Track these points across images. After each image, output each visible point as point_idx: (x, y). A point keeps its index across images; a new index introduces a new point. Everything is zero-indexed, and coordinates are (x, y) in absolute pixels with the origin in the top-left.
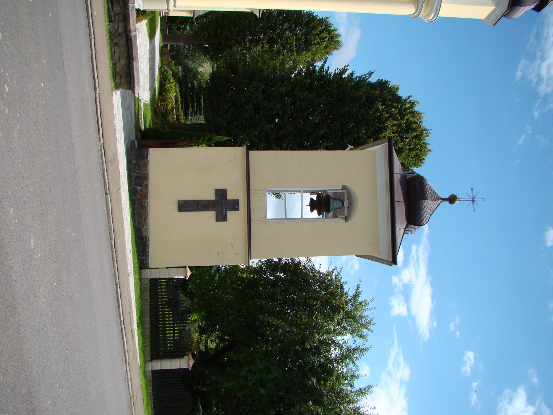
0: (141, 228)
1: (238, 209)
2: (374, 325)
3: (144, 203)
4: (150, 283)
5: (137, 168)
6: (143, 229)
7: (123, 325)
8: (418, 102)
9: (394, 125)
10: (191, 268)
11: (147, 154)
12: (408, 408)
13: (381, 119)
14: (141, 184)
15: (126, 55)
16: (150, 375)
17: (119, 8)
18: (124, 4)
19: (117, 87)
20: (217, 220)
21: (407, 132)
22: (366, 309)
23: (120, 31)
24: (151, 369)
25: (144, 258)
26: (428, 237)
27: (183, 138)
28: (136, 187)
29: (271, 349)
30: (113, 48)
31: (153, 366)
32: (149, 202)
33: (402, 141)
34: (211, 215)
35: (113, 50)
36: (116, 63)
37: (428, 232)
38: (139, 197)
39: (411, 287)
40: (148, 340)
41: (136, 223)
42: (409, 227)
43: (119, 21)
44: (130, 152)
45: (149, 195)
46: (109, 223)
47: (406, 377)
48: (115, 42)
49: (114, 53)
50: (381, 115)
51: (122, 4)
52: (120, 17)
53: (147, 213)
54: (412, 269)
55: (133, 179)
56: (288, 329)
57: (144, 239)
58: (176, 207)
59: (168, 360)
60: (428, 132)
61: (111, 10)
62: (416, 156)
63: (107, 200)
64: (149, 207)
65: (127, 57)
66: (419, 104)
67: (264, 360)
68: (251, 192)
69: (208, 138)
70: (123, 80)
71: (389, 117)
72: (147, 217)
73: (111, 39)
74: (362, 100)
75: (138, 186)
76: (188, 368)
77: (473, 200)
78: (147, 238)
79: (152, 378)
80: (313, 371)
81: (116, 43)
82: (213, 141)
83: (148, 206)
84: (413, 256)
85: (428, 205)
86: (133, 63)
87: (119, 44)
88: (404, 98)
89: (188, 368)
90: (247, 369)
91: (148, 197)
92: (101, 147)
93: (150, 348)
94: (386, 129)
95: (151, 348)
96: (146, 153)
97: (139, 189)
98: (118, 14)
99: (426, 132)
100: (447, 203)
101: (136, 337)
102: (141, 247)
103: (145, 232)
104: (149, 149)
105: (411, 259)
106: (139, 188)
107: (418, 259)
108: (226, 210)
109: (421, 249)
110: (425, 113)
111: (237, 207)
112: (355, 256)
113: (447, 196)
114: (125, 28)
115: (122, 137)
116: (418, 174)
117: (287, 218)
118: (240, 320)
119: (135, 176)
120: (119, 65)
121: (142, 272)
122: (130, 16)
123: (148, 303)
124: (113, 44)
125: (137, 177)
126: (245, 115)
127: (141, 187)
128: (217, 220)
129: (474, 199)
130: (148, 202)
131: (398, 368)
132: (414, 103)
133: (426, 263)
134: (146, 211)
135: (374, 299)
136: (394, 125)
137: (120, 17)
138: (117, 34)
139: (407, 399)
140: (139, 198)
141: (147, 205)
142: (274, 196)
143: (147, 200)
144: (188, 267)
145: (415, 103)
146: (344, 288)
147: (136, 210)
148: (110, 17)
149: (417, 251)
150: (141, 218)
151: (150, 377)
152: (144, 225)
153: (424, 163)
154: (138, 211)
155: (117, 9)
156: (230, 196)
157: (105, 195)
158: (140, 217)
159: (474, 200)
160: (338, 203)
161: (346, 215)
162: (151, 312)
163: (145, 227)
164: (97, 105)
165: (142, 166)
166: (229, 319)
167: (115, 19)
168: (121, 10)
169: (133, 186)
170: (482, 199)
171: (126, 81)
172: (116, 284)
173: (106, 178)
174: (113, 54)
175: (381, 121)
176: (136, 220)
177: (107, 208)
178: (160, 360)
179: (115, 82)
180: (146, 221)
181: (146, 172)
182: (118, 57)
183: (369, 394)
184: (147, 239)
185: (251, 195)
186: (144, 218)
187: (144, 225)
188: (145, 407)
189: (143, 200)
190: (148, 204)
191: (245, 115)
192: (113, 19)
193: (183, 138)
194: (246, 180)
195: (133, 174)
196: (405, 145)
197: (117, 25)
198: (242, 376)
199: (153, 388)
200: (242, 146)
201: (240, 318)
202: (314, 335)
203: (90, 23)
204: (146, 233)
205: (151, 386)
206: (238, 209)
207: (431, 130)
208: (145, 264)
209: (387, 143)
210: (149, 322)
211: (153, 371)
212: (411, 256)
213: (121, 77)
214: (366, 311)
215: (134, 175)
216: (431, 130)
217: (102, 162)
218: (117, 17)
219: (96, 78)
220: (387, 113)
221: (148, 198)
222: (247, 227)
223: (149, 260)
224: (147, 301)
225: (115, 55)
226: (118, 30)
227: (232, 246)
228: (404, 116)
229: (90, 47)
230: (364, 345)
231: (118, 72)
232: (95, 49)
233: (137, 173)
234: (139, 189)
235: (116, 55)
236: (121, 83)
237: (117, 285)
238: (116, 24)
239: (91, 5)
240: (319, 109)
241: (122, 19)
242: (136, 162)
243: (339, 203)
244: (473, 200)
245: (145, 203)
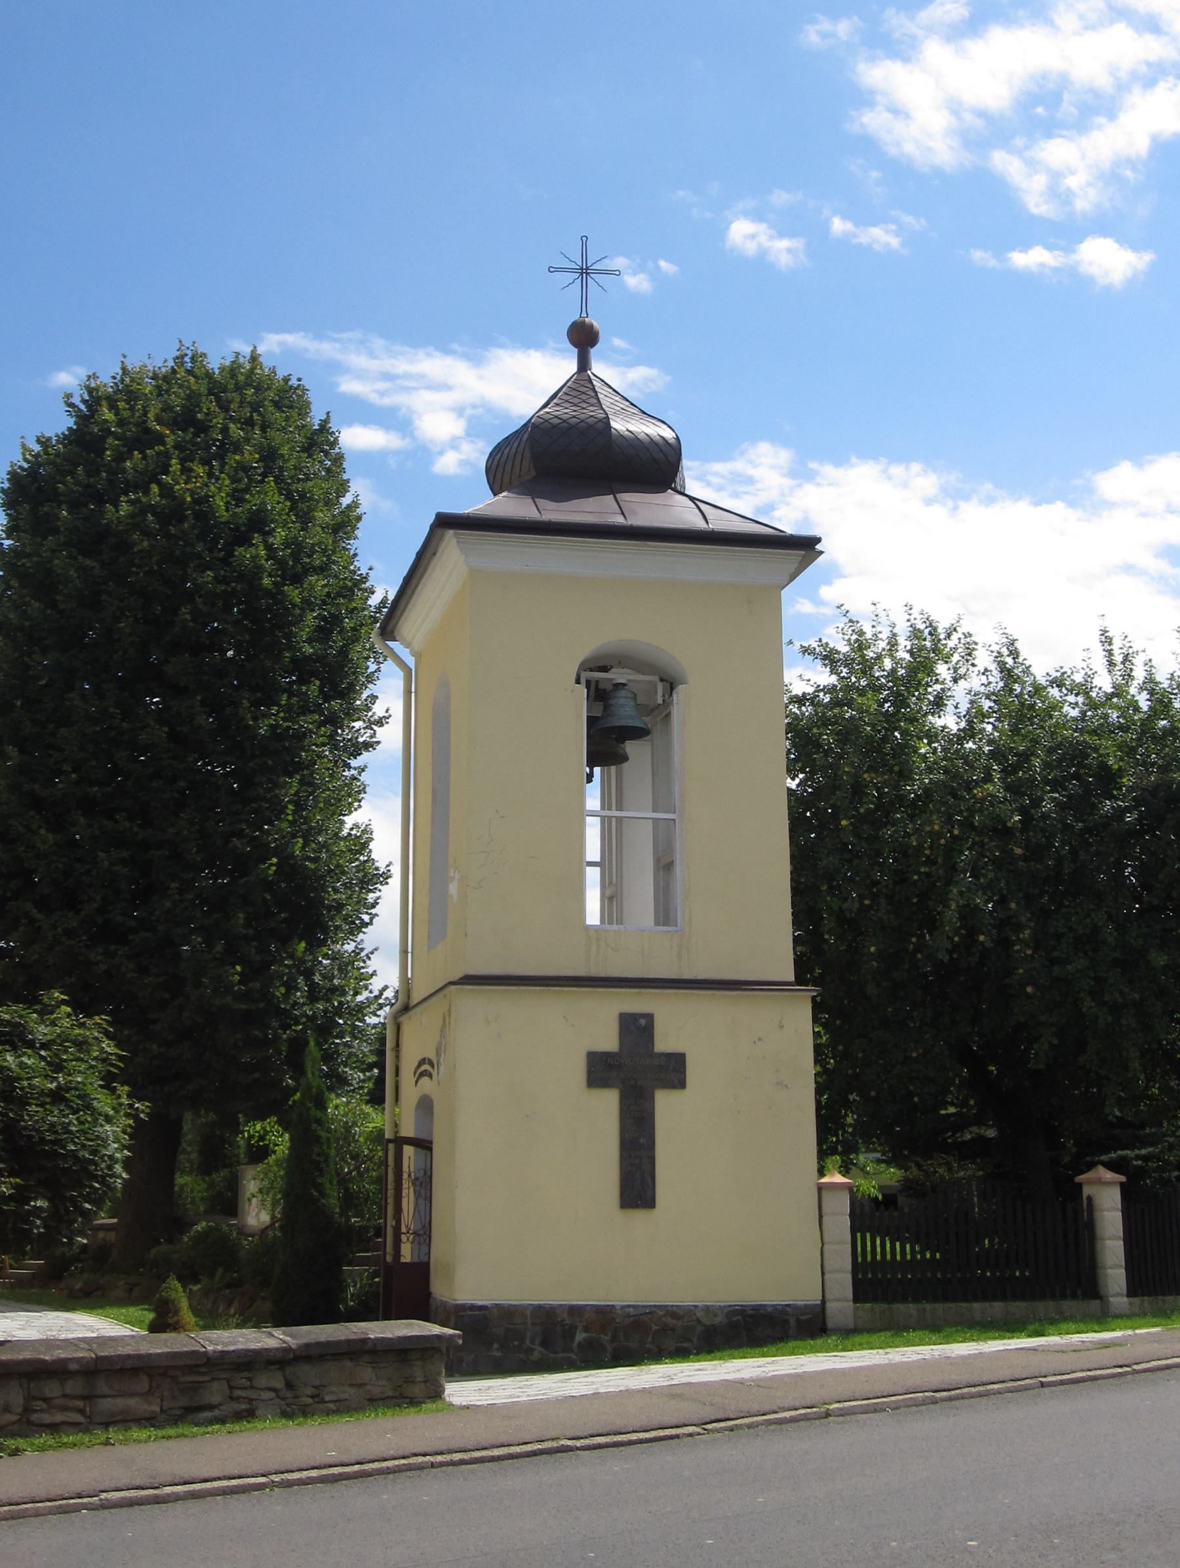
0: (703, 1328)
1: (650, 1018)
2: (911, 609)
3: (627, 1321)
4: (865, 1301)
5: (516, 1343)
7: (1135, 1367)
8: (89, 377)
9: (187, 471)
11: (473, 1307)
12: (884, 460)
13: (167, 511)
14: (567, 1327)
15: (348, 1364)
16: (1137, 1300)
17: (216, 1386)
18: (203, 1370)
20: (682, 1085)
21: (203, 428)
22: (874, 629)
23: (279, 1383)
24: (1125, 1299)
25: (792, 1322)
26: (320, 337)
27: (315, 1193)
28: (575, 1344)
29: (1027, 932)
30: (326, 1405)
31: (1119, 1291)
32: (622, 1304)
33: (237, 449)
34: (665, 1102)
35: (332, 1406)
36: (369, 1397)
37: (302, 334)
38: (606, 1334)
39: (480, 410)
40: (1067, 1305)
41: (686, 1345)
43: (252, 1387)
44: (464, 1364)
45: (603, 1303)
46: (898, 1405)
47: (784, 456)
48: (310, 1401)
49: (342, 1403)
50: (152, 509)
51: (203, 1374)
52: (240, 1382)
53: (654, 1309)
54: (421, 400)
55: (552, 1355)
56: (969, 877)
57: (735, 1319)
58: (639, 1217)
59: (1099, 1245)
60: (187, 355)
61: (217, 1412)
62: (277, 405)
63: (842, 1413)
64: (640, 1303)
65: (351, 1359)
66: (97, 375)
67: (1056, 954)
68: (594, 972)
69: (313, 1109)
70: (418, 1373)
71: (159, 483)
72: (669, 1308)
73: (305, 1412)
74: (93, 568)
75: (573, 1337)
76: (1122, 1184)
78: (732, 1308)
79: (1146, 1296)
80: (1081, 805)
81: (312, 1397)
82: (322, 1091)
83: (633, 1306)
84: (377, 391)
86: (376, 1339)
87: (316, 1387)
88: (71, 422)
89: (1122, 1184)
90: (1089, 1002)
91: (608, 1306)
92: (712, 1431)
93: (1062, 1302)
94: (202, 501)
95: (1064, 1297)
96: (469, 1313)
97: (584, 1335)
98: (231, 1388)
99: (187, 359)
100: (593, 352)
101: (1047, 1341)
102: (760, 1329)
103: (716, 1315)
105: (387, 401)
106: (580, 1336)
107: (388, 376)
108: (651, 1054)
109: (359, 361)
110: (125, 357)
111: (643, 1022)
114: (272, 1367)
115: (590, 1379)
117: (599, 860)
118: (918, 1024)
119: (542, 1350)
120: (374, 1385)
121: (834, 1326)
122: (242, 1350)
123: (928, 1306)
124: (316, 1405)
125: (546, 1343)
126: (128, 975)
127: (576, 1328)
128: (682, 1085)
130: (623, 1307)
131: (750, 481)
132: (90, 391)
133: (407, 349)
134: (652, 1312)
135: (841, 603)
136: (187, 471)
137: (240, 1382)
138: (288, 1394)
139: (854, 460)
140: (610, 1334)
141: (631, 1310)
142: (380, 890)
143: (617, 1308)
144: (819, 1179)
145: (93, 385)
146: (800, 693)
147: (648, 1346)
148: (238, 1417)
149: (361, 376)
150: (673, 1330)
151: (1143, 1301)
152: (694, 1318)
153: (299, 380)
154: (650, 1340)
155: (215, 1393)
156: (608, 1041)
157: (832, 1418)
158: (669, 1332)
160: (622, 701)
161: (656, 678)
162: (955, 1299)
163: (700, 1314)
164: (641, 1441)
166: (917, 1057)
167: (246, 1400)
168: (219, 1379)
169: (574, 1356)
170: (584, 240)
171: (419, 1363)
172: (1042, 1386)
173: (787, 1416)
174: (342, 1408)
175: (173, 512)
176: (680, 1345)
177: (861, 1413)
178: (1099, 1271)
179: (422, 1400)
180: (681, 1313)
181: (528, 1312)
182: (352, 1391)
183: (1130, 642)
184: (736, 1310)
185: (602, 974)
186: (673, 1318)
187: (694, 1318)
188: (51, 1442)
189: (618, 1321)
190: (629, 1306)
191: (128, 975)
192: (244, 1407)
193: (315, 1193)
194: (561, 989)
195: (536, 1356)
196: (247, 440)
197: (262, 1393)
198: (1110, 1019)
199: (1170, 1294)
201: (912, 1025)
202: (981, 799)
203: (388, 1468)
204: (720, 1312)
205: (1165, 1298)
206: (650, 1018)
207: (180, 342)
208: (810, 1316)
210: (987, 1304)
211: (1129, 1295)
212: (374, 398)
213: (409, 1380)
214: (880, 632)
215: (538, 1352)
216: (180, 342)
217: (749, 1426)
218: (238, 1393)
219: (529, 1448)
220: (147, 492)
221: (613, 1306)
222: (728, 993)
223: (799, 1303)
224: (924, 1310)
225: (346, 1400)
226: (275, 1390)
227: (760, 1039)
228: (147, 431)
229: (456, 1468)
230: (990, 646)
231: (395, 1389)
232: (450, 1452)
233: (532, 1342)
234: (584, 1335)
235: (346, 1396)
236: (425, 1382)
237: (1042, 1385)
238: (260, 1395)
239: (331, 1466)
240: (118, 721)
241: (245, 1374)
242: (496, 1346)
243: (622, 697)
245: (629, 1316)
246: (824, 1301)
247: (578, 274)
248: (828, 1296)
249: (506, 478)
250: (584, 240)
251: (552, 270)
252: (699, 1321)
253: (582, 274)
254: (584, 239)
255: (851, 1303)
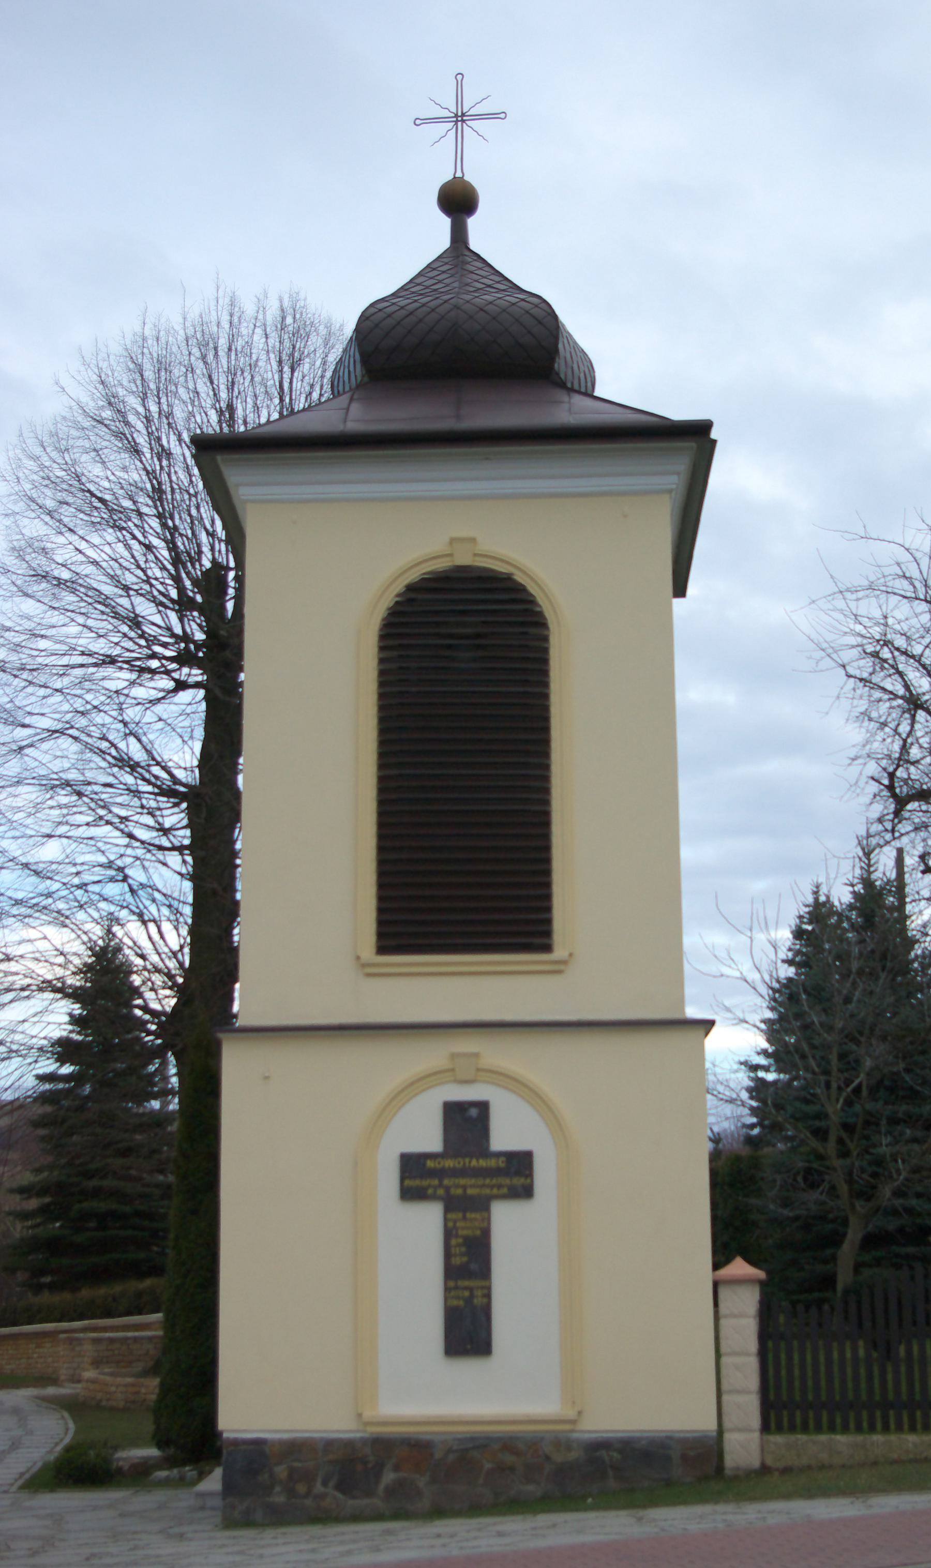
4: (780, 1429)
6: (558, 1458)
10: (720, 1259)
14: (370, 1465)
16: (778, 1439)
19: (242, 682)
42: (562, 376)
76: (762, 1284)
77: (460, 118)
85: (859, 877)
100: (472, 222)
104: (225, 1435)
111: (474, 1112)
112: (680, 590)
113: (445, 222)
116: (351, 338)
129: (456, 116)
159: (456, 122)
165: (297, 1465)
170: (459, 78)
200: (218, 1045)
206: (483, 1107)
209: (219, 458)
242: (278, 1489)
244: (460, 118)
246: (720, 1431)
247: (464, 124)
248: (727, 1424)
249: (341, 388)
250: (459, 78)
251: (418, 122)
252: (548, 1458)
253: (456, 122)
254: (459, 77)
255: (756, 1435)
